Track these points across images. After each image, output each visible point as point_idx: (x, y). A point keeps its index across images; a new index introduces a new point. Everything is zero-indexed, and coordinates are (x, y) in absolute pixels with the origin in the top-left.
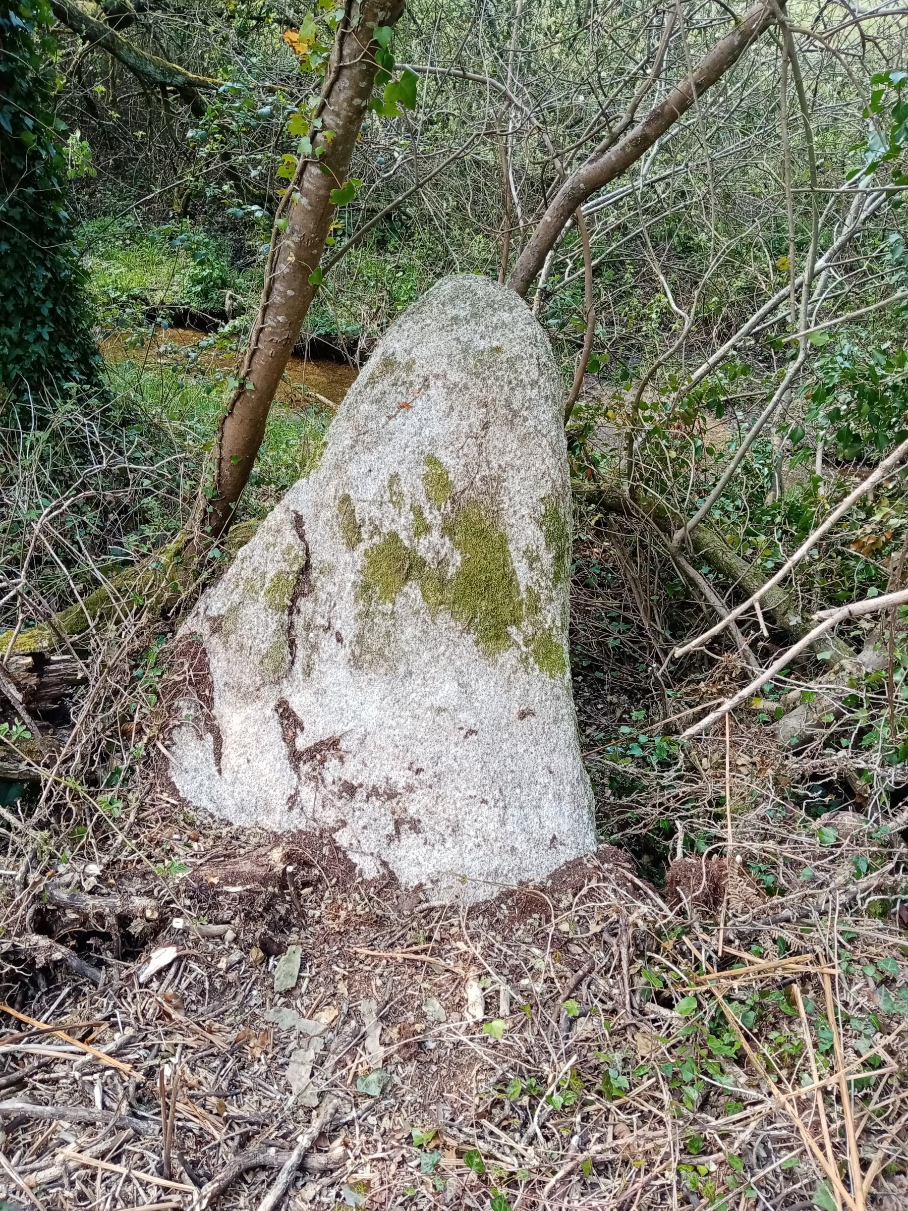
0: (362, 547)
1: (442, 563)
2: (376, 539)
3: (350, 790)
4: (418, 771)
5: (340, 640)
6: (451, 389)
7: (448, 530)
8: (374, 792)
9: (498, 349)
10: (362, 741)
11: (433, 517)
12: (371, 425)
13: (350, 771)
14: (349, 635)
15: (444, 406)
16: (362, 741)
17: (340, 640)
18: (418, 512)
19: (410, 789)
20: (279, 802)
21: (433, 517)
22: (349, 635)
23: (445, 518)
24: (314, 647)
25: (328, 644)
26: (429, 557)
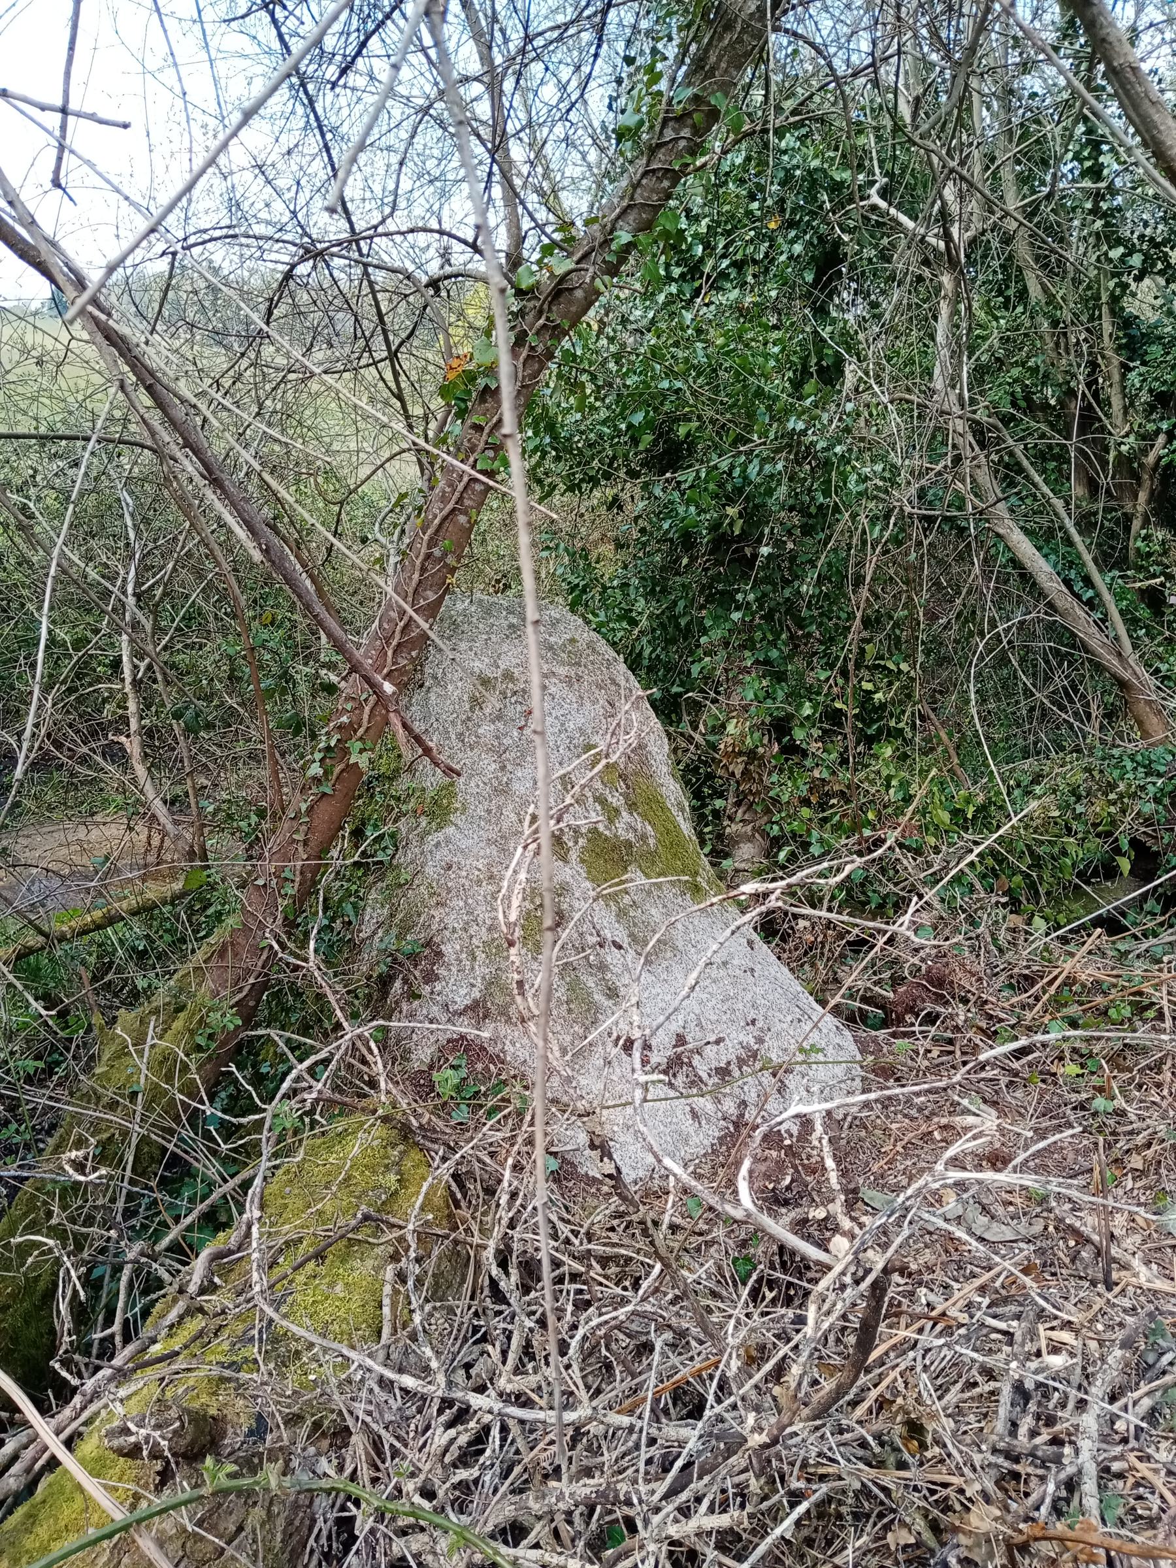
0: (573, 856)
1: (643, 837)
2: (582, 842)
3: (723, 1072)
4: (753, 1022)
5: (620, 947)
6: (568, 681)
7: (632, 807)
8: (741, 1062)
9: (573, 641)
10: (699, 1024)
11: (616, 800)
12: (507, 741)
13: (715, 1057)
14: (622, 937)
15: (572, 697)
16: (699, 1024)
17: (620, 947)
18: (601, 800)
19: (760, 1040)
20: (688, 1125)
21: (616, 800)
22: (622, 937)
23: (626, 796)
24: (603, 967)
25: (612, 957)
26: (631, 836)
